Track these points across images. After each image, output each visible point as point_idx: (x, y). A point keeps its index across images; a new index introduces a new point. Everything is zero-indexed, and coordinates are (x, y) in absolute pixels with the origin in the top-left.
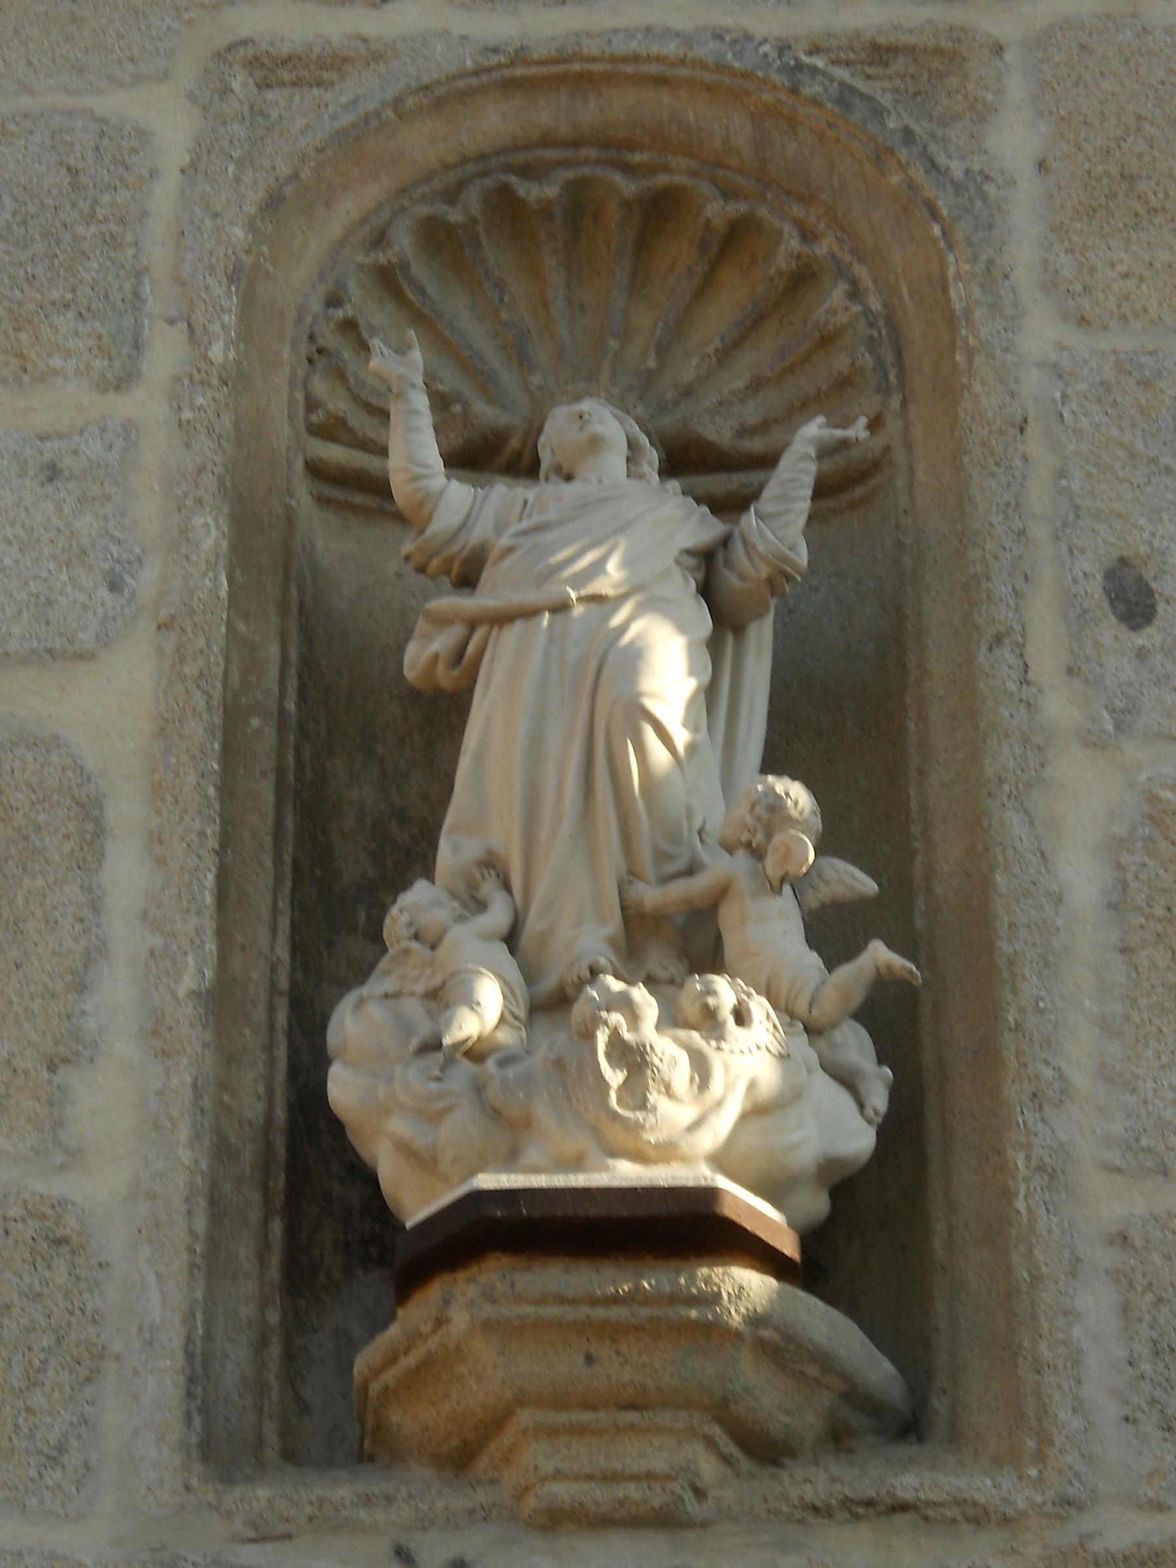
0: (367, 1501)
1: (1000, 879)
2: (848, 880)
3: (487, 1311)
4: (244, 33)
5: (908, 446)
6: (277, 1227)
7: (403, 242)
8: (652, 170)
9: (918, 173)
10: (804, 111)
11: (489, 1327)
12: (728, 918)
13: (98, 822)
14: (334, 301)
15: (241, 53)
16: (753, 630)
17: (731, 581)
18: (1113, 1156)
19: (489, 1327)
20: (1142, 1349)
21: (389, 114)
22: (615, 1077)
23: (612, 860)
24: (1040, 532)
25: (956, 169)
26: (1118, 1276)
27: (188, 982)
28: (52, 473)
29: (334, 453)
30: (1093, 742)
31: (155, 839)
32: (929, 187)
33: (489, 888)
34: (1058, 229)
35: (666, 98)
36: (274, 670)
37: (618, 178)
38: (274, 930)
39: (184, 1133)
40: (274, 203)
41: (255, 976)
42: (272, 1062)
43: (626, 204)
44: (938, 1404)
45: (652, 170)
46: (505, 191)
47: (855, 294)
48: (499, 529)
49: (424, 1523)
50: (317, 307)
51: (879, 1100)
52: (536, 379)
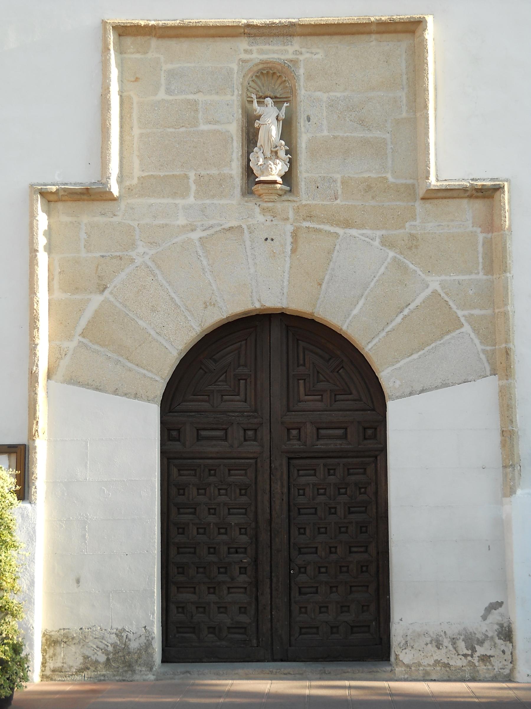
0: (253, 199)
1: (298, 145)
3: (261, 188)
4: (241, 58)
7: (254, 77)
8: (273, 70)
9: (294, 75)
10: (285, 67)
11: (261, 189)
13: (233, 139)
14: (249, 84)
15: (241, 60)
16: (280, 122)
17: (279, 118)
18: (305, 171)
19: (261, 189)
20: (306, 188)
22: (270, 170)
23: (270, 147)
24: (302, 112)
25: (297, 74)
26: (305, 181)
27: (240, 155)
28: (228, 105)
29: (249, 99)
30: (305, 133)
31: (237, 141)
32: (295, 76)
33: (261, 147)
34: (305, 81)
35: (274, 64)
37: (271, 71)
39: (240, 168)
40: (244, 76)
43: (271, 73)
44: (292, 189)
45: (273, 70)
46: (262, 72)
47: (289, 84)
48: (262, 113)
49: (257, 201)
50: (247, 84)
51: (289, 166)
52: (264, 88)
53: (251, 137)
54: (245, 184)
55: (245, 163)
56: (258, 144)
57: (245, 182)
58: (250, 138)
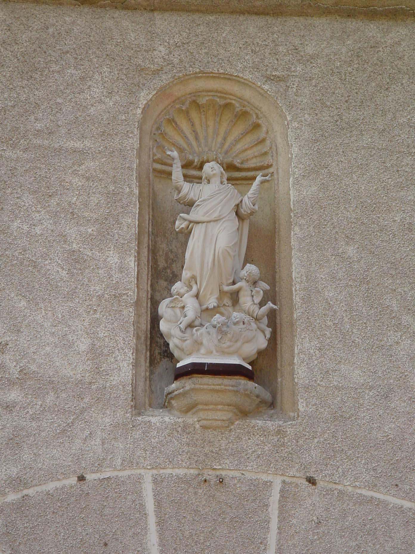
2: (264, 286)
5: (278, 173)
6: (148, 353)
12: (241, 294)
21: (171, 84)
29: (159, 167)
33: (193, 283)
36: (147, 222)
38: (147, 284)
41: (144, 296)
42: (147, 316)
48: (194, 196)
51: (268, 336)
53: (162, 264)
54: (143, 379)
55: (145, 324)
56: (186, 274)
57: (143, 374)
58: (158, 266)
